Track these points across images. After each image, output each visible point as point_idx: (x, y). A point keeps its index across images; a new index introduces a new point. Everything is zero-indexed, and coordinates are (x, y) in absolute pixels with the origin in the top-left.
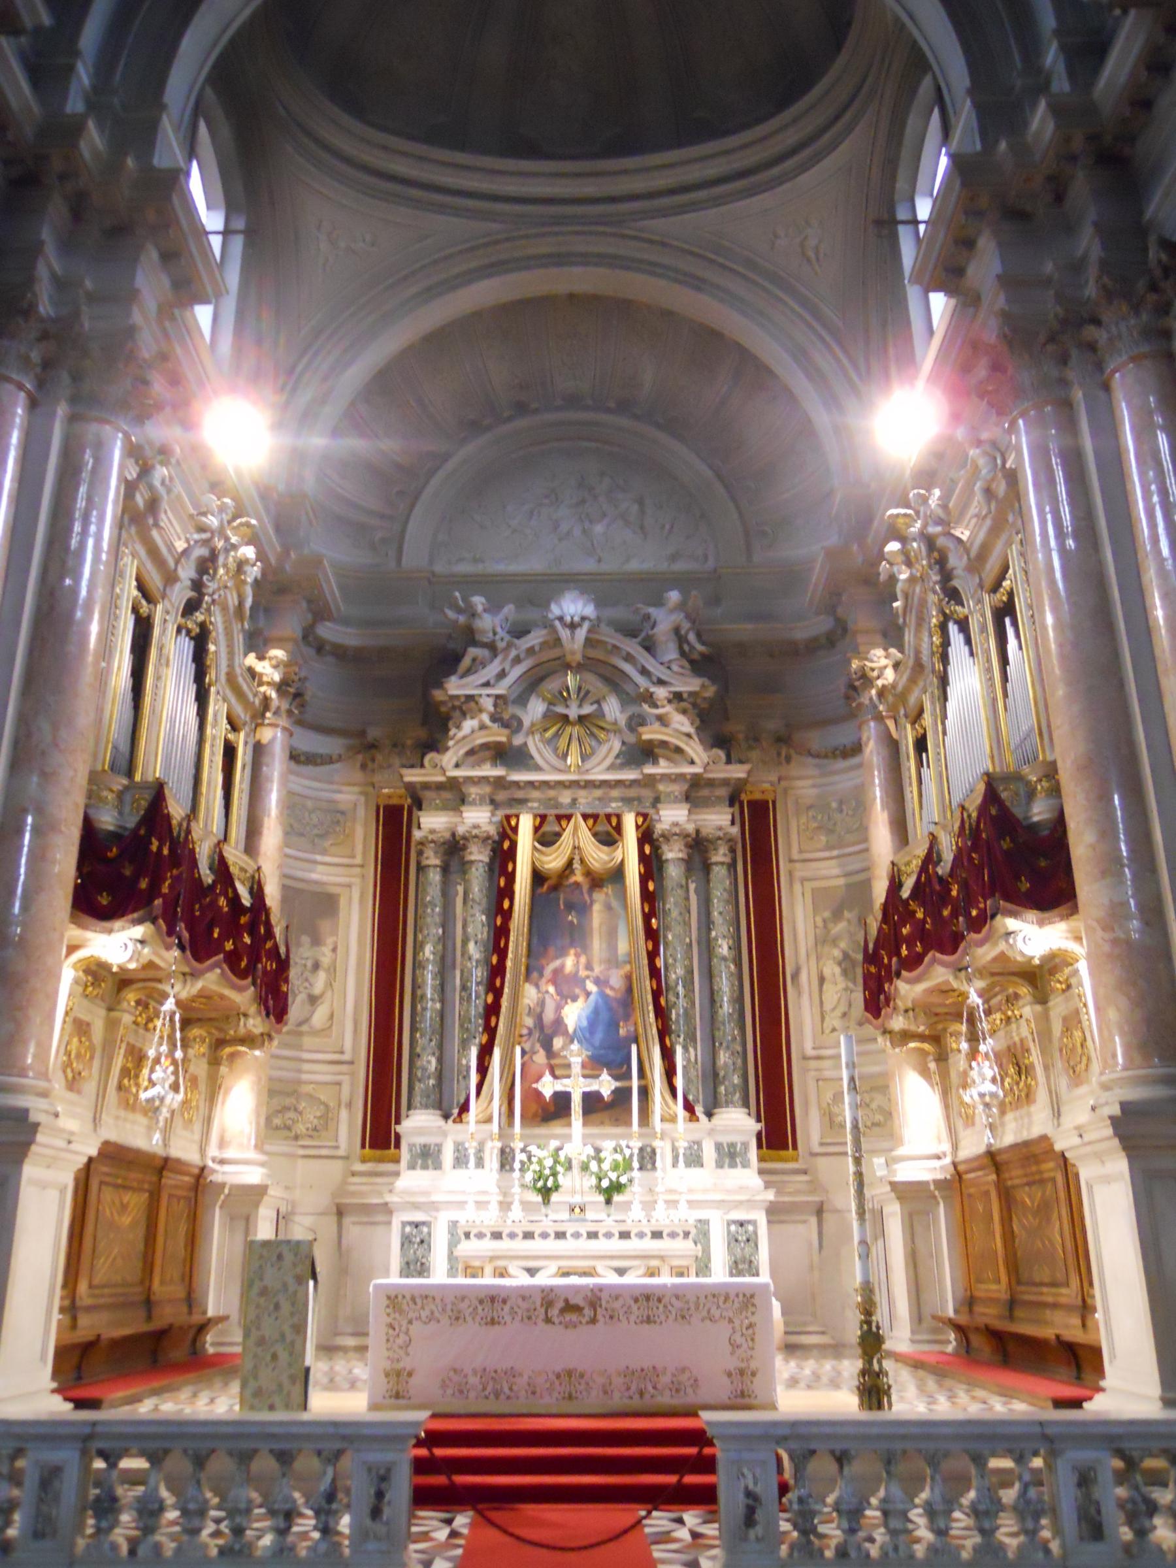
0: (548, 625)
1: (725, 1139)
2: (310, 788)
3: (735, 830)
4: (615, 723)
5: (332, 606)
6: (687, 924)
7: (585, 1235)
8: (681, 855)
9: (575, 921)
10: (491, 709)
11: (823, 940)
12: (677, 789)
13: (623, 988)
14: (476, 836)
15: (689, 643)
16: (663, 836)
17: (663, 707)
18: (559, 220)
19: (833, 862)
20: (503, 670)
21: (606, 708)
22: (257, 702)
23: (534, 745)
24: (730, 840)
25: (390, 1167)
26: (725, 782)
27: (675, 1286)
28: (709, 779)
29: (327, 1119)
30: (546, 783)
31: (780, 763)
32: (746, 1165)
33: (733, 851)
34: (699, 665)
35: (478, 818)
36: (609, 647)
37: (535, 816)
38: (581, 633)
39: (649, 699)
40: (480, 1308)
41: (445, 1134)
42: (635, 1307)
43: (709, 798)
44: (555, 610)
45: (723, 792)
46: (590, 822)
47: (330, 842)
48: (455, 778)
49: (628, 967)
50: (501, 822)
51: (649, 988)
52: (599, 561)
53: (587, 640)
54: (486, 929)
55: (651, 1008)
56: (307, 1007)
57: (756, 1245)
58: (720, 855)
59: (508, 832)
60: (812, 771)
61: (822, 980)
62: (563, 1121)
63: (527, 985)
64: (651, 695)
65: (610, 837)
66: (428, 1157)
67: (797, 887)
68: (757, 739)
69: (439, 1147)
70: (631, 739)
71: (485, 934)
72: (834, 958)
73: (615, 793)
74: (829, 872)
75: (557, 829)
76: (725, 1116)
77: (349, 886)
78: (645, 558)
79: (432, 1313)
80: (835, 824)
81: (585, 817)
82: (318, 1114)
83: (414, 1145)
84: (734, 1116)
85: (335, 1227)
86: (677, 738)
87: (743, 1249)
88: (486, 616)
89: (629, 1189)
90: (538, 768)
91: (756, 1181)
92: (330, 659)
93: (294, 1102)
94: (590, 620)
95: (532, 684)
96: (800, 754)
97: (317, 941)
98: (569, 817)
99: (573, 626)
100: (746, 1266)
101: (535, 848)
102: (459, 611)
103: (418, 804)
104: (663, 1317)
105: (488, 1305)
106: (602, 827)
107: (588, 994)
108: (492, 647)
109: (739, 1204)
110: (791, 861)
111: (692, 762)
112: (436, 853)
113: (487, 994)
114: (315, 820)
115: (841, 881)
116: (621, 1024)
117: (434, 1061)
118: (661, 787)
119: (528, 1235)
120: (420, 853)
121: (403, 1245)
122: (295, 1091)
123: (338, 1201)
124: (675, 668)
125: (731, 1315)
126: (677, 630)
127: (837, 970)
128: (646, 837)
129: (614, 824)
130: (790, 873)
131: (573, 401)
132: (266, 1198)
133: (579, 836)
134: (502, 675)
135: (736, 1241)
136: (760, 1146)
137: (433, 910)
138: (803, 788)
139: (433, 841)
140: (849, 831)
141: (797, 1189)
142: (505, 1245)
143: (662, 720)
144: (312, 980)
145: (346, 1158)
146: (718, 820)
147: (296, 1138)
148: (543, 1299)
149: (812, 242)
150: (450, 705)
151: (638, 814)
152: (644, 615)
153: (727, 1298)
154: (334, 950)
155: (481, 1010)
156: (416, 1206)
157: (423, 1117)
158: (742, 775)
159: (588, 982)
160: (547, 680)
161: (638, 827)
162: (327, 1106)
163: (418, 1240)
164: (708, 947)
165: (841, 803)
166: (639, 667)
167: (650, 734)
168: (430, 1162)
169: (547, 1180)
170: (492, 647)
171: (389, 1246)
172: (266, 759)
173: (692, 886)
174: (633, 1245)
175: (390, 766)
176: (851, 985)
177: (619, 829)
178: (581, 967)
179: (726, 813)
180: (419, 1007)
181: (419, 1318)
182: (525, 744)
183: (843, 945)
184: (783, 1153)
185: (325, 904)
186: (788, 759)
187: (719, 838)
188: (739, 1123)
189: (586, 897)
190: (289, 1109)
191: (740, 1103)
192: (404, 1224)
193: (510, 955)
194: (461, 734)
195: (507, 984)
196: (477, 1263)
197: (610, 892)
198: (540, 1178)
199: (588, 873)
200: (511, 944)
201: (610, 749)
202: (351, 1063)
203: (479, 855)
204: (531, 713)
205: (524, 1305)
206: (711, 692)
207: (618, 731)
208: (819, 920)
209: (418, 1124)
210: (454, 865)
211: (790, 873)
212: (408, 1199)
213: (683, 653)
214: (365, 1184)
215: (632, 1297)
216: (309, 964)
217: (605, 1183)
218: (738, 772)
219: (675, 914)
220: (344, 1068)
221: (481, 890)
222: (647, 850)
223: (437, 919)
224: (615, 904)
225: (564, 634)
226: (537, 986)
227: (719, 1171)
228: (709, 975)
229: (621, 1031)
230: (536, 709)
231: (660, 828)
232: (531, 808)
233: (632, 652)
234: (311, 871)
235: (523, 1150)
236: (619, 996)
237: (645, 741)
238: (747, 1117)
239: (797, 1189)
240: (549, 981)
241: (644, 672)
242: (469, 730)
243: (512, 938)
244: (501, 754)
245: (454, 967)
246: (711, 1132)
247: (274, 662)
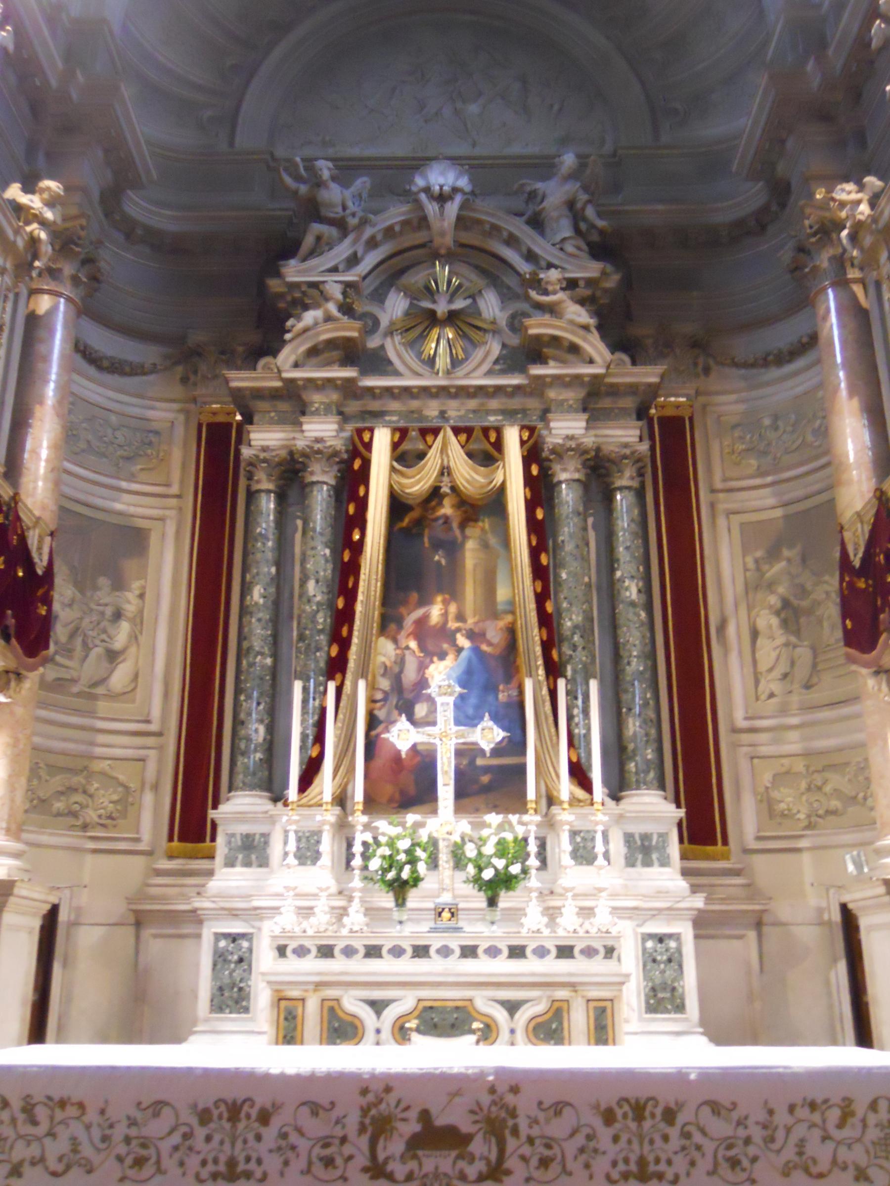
1: (637, 829)
2: (109, 399)
4: (494, 322)
5: (137, 160)
6: (585, 559)
7: (458, 952)
8: (576, 476)
9: (443, 562)
10: (340, 297)
11: (756, 585)
12: (572, 395)
13: (503, 644)
14: (319, 452)
15: (585, 219)
16: (553, 451)
17: (555, 293)
19: (767, 490)
20: (355, 254)
21: (481, 304)
22: (20, 243)
23: (394, 349)
25: (203, 864)
26: (632, 389)
27: (708, 1077)
28: (612, 385)
29: (126, 803)
30: (406, 390)
31: (697, 376)
32: (664, 862)
33: (641, 474)
34: (600, 249)
35: (322, 429)
36: (487, 227)
37: (394, 430)
38: (452, 208)
39: (536, 283)
40: (200, 1133)
41: (272, 820)
42: (605, 1134)
43: (612, 409)
44: (420, 182)
45: (629, 403)
46: (463, 437)
47: (139, 467)
48: (292, 381)
49: (509, 618)
50: (351, 439)
51: (537, 638)
52: (474, 145)
53: (459, 218)
54: (330, 566)
55: (540, 662)
56: (105, 664)
57: (680, 966)
58: (626, 478)
61: (755, 634)
62: (427, 807)
63: (382, 640)
64: (540, 281)
65: (488, 455)
66: (253, 850)
67: (722, 522)
69: (266, 836)
70: (514, 341)
71: (329, 572)
72: (770, 607)
73: (494, 404)
74: (763, 502)
75: (421, 446)
76: (635, 800)
77: (162, 519)
78: (528, 142)
79: (75, 1143)
80: (769, 444)
81: (457, 431)
82: (115, 797)
83: (233, 835)
84: (647, 799)
85: (132, 940)
86: (573, 333)
87: (663, 972)
88: (333, 186)
89: (522, 884)
90: (397, 374)
91: (682, 884)
93: (83, 781)
94: (464, 193)
95: (392, 274)
96: (722, 364)
97: (119, 585)
98: (436, 431)
99: (442, 198)
100: (668, 995)
101: (393, 469)
102: (298, 178)
103: (249, 419)
104: (680, 1164)
105: (221, 1127)
107: (459, 650)
108: (341, 225)
109: (656, 913)
110: (713, 491)
111: (591, 361)
112: (269, 475)
113: (330, 646)
114: (121, 440)
115: (779, 513)
116: (501, 687)
117: (262, 729)
118: (552, 394)
119: (373, 952)
120: (250, 477)
121: (215, 965)
122: (86, 768)
123: (134, 907)
124: (569, 248)
125: (863, 1161)
126: (571, 204)
127: (775, 621)
128: (532, 454)
129: (493, 440)
130: (712, 506)
132: (12, 899)
133: (450, 456)
134: (353, 261)
135: (654, 961)
136: (681, 841)
137: (264, 544)
138: (725, 404)
139: (265, 461)
140: (787, 452)
142: (337, 965)
144: (111, 631)
145: (149, 853)
146: (624, 435)
147: (85, 827)
148: (365, 1111)
150: (289, 298)
151: (523, 428)
152: (530, 193)
153: (847, 1114)
154: (142, 596)
155: (322, 664)
156: (234, 914)
157: (247, 800)
158: (654, 380)
159: (459, 636)
160: (412, 271)
161: (523, 443)
162: (126, 787)
163: (236, 957)
164: (609, 590)
165: (776, 418)
166: (524, 249)
167: (539, 326)
168: (253, 857)
169: (401, 869)
170: (341, 225)
171: (197, 965)
172: (42, 333)
173: (590, 520)
174: (530, 966)
175: (216, 377)
176: (793, 639)
177: (499, 445)
178: (451, 617)
179: (635, 428)
180: (244, 662)
181: (39, 1161)
182: (382, 347)
183: (781, 590)
184: (709, 848)
185: (133, 539)
186: (707, 371)
187: (625, 457)
188: (655, 810)
189: (457, 532)
190: (76, 790)
191: (655, 783)
192: (218, 936)
193: (360, 597)
194: (300, 326)
195: (356, 633)
196: (295, 993)
197: (487, 526)
198: (391, 867)
200: (361, 583)
201: (488, 354)
202: (159, 734)
203: (322, 478)
204: (389, 310)
205: (316, 1127)
206: (613, 281)
207: (496, 332)
208: (750, 560)
210: (293, 494)
211: (712, 506)
212: (223, 905)
213: (578, 231)
214: (174, 886)
215: (597, 1106)
216: (109, 611)
217: (488, 874)
219: (569, 547)
220: (150, 741)
221: (324, 518)
222: (535, 470)
223: (270, 555)
224: (493, 541)
225: (431, 208)
226: (395, 641)
227: (630, 870)
228: (613, 626)
229: (501, 696)
230: (396, 306)
232: (390, 422)
233: (517, 233)
234: (114, 500)
235: (367, 827)
236: (498, 651)
237: (531, 336)
238: (664, 801)
240: (409, 635)
243: (362, 577)
244: (349, 352)
245: (291, 618)
246: (620, 818)
247: (46, 196)
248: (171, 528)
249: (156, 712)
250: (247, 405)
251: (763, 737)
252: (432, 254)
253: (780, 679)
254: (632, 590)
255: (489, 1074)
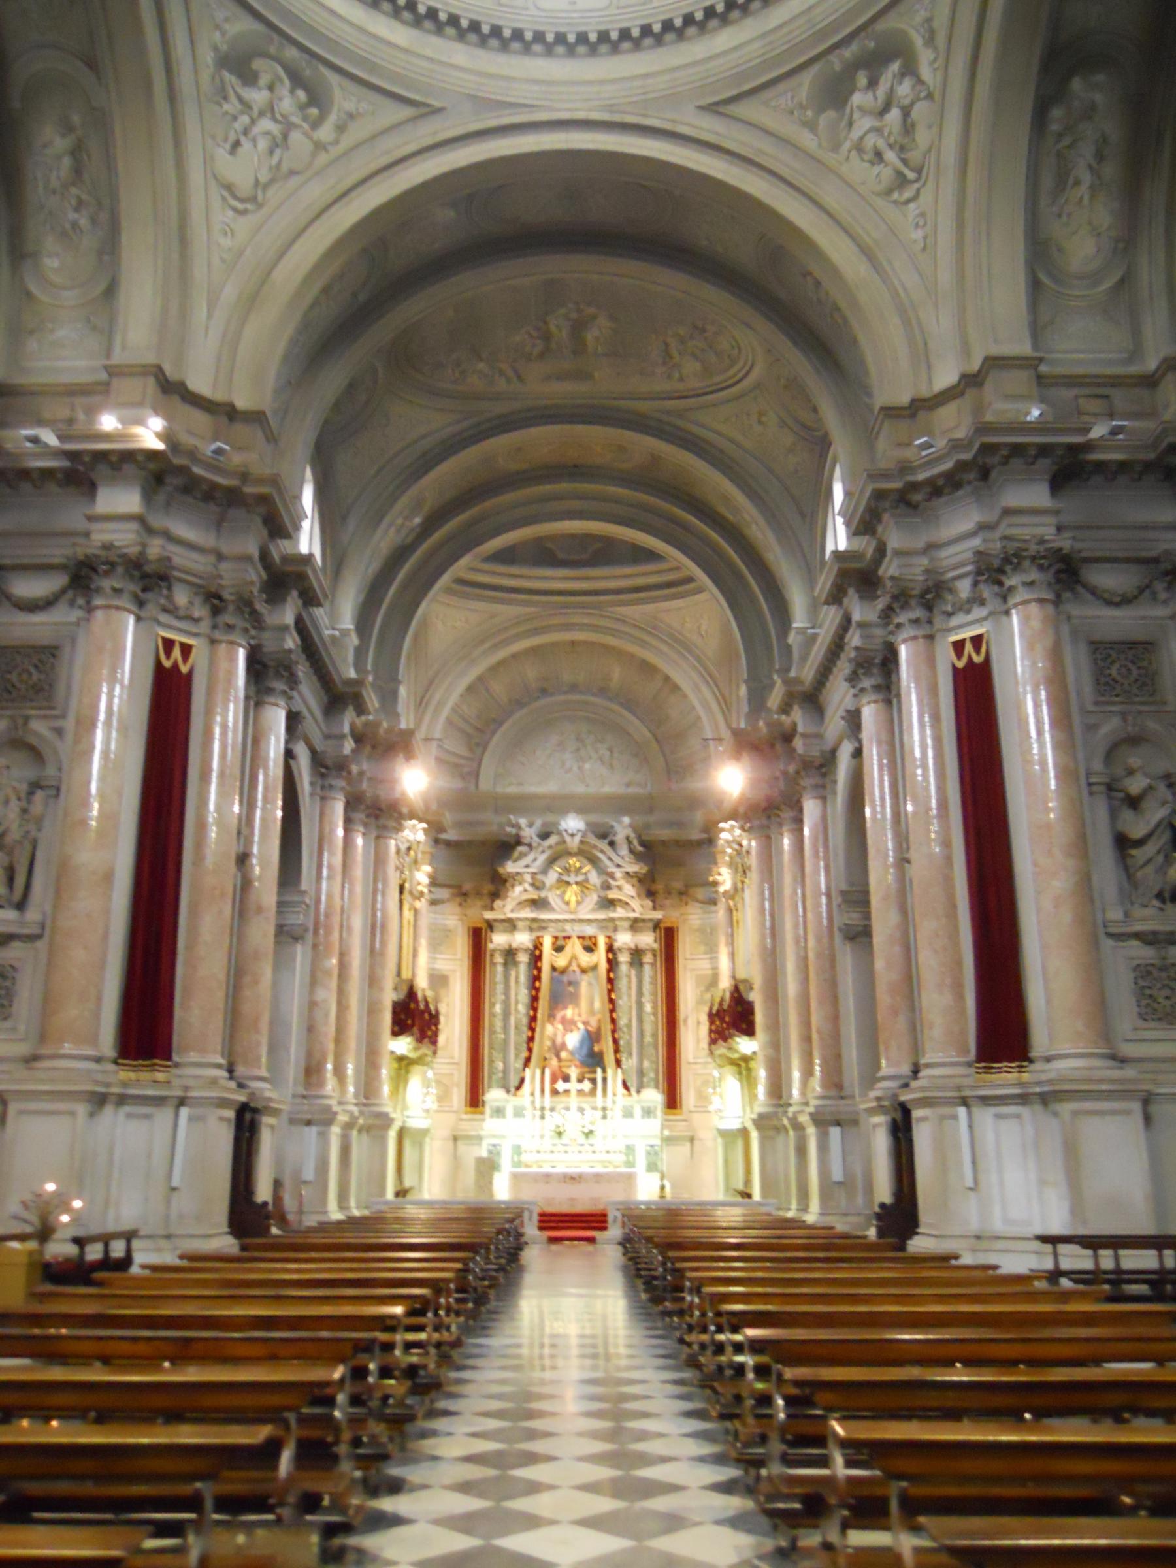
0: (559, 833)
1: (646, 1105)
3: (656, 946)
12: (626, 924)
18: (565, 606)
24: (654, 952)
26: (651, 920)
30: (559, 920)
33: (655, 956)
34: (638, 857)
35: (523, 939)
38: (577, 839)
41: (507, 1101)
45: (651, 925)
58: (648, 958)
59: (538, 946)
60: (700, 911)
61: (699, 1023)
66: (499, 1112)
68: (670, 893)
69: (504, 1108)
70: (603, 894)
77: (454, 971)
90: (553, 910)
92: (442, 846)
95: (552, 861)
99: (572, 835)
102: (513, 826)
106: (588, 943)
120: (492, 955)
128: (610, 949)
131: (574, 688)
134: (535, 860)
141: (680, 1129)
143: (619, 888)
146: (648, 940)
149: (704, 627)
156: (494, 1136)
164: (640, 1005)
167: (612, 895)
170: (530, 846)
177: (595, 944)
186: (686, 904)
188: (654, 1097)
199: (579, 966)
203: (523, 958)
209: (493, 1096)
218: (658, 915)
224: (593, 982)
225: (568, 839)
230: (552, 877)
231: (616, 945)
239: (680, 1129)
241: (610, 859)
242: (518, 892)
248: (458, 974)
249: (456, 1055)
250: (490, 925)
251: (698, 1066)
252: (569, 854)
253: (1147, 740)
254: (648, 1008)
255: (640, 1301)
